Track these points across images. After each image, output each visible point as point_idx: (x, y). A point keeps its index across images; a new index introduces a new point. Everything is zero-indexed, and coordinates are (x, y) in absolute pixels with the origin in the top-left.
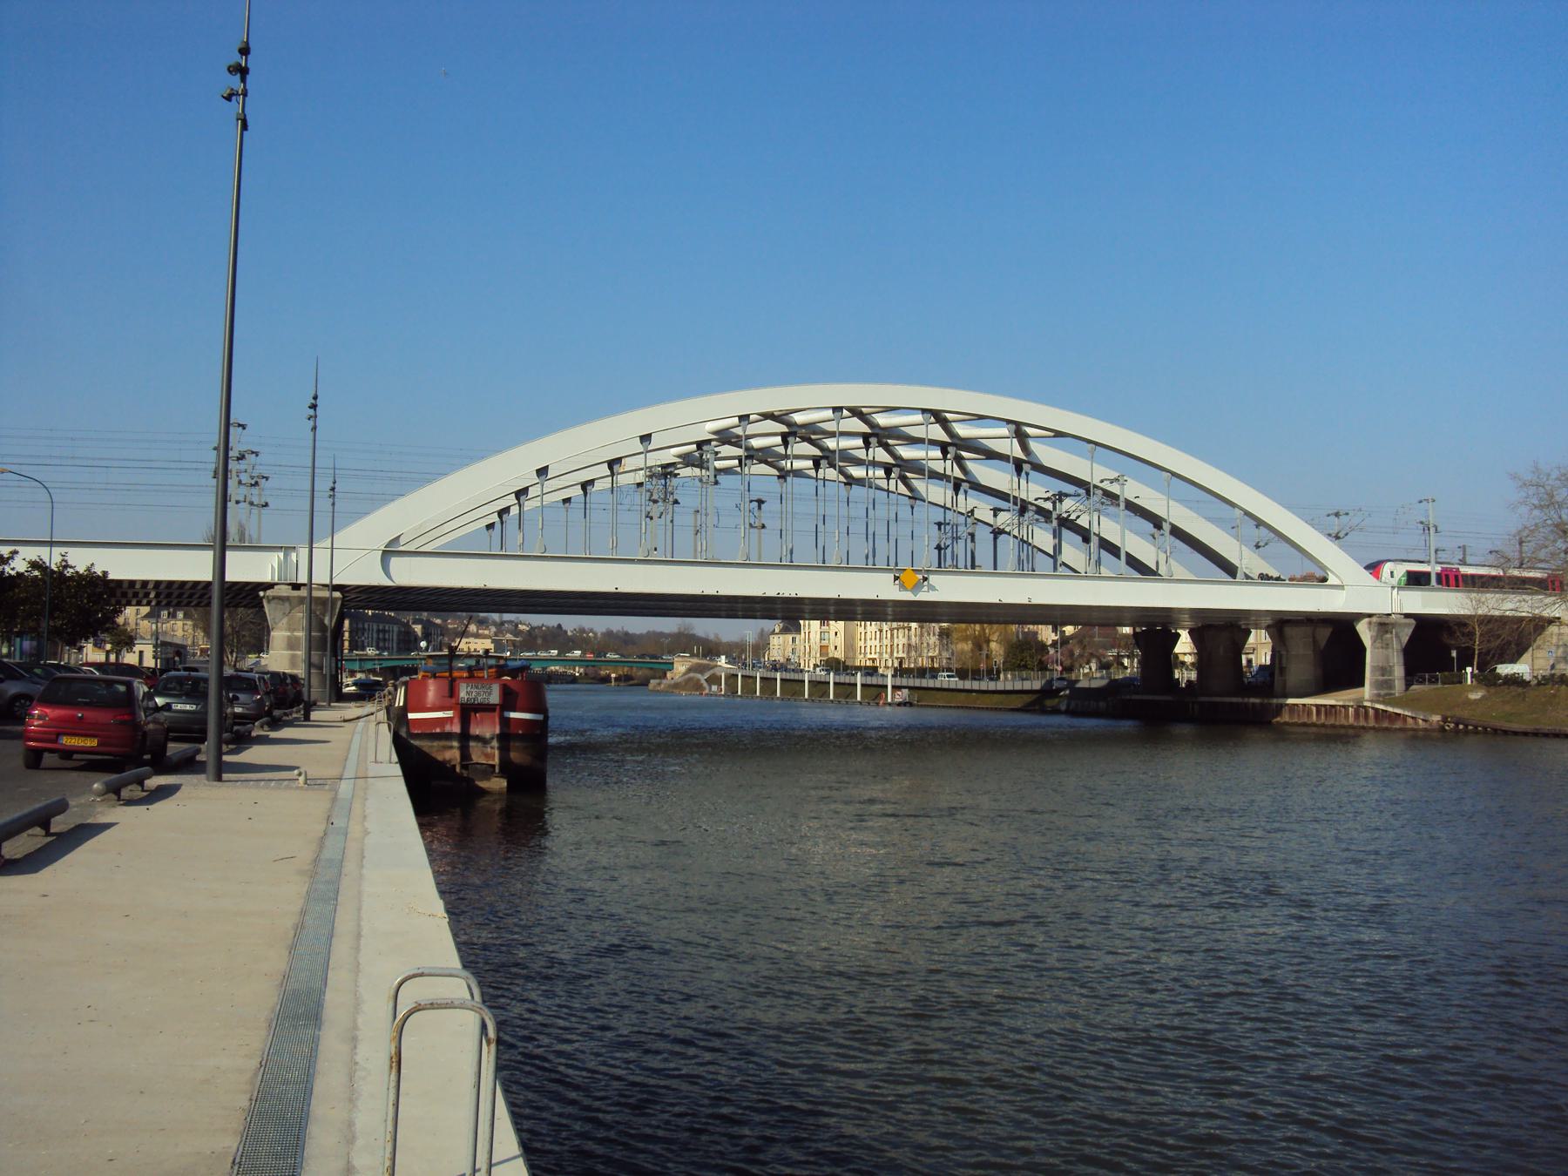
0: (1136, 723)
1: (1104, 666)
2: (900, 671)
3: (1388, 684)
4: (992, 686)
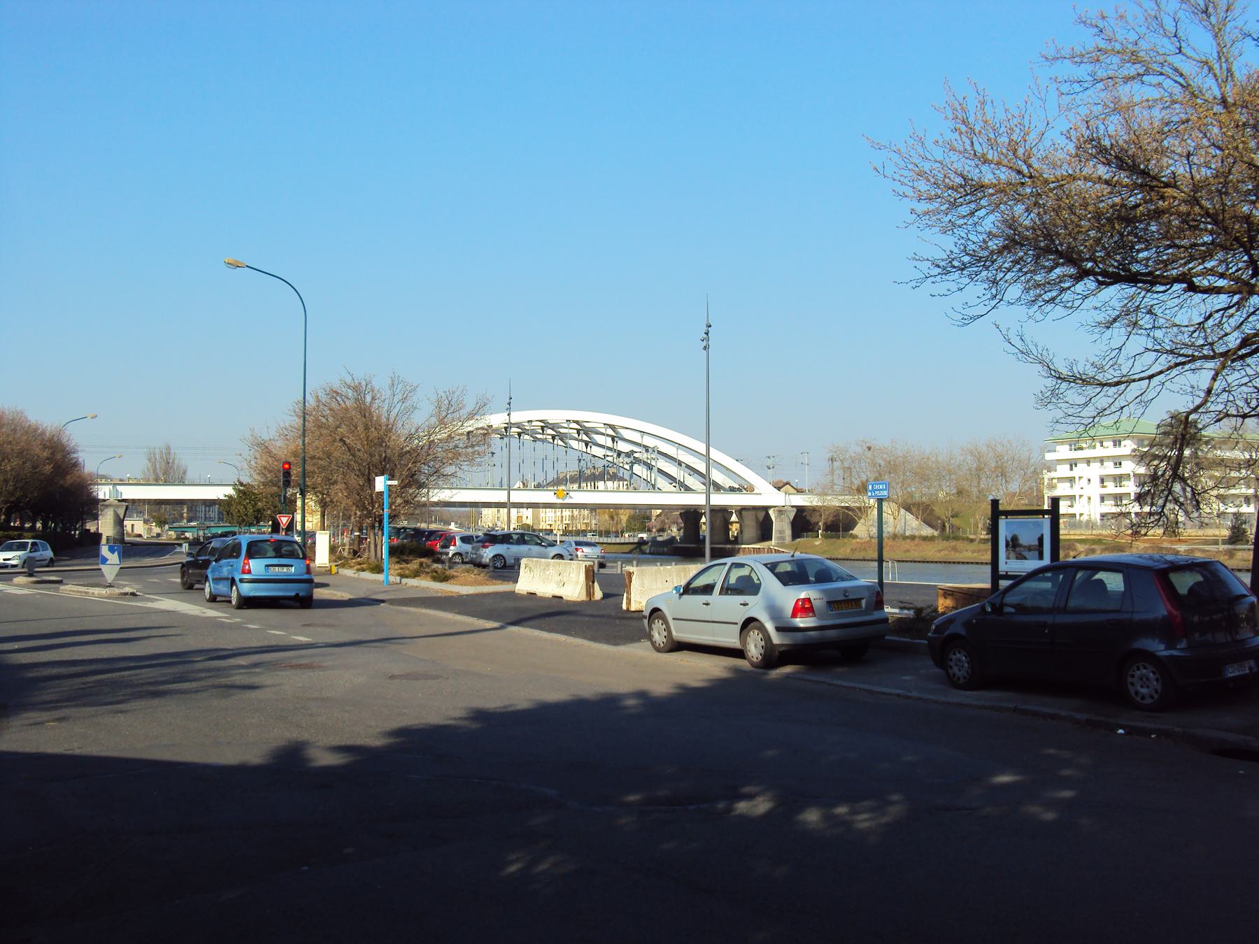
0: (1122, 589)
1: (276, 528)
2: (566, 533)
3: (783, 538)
4: (618, 540)
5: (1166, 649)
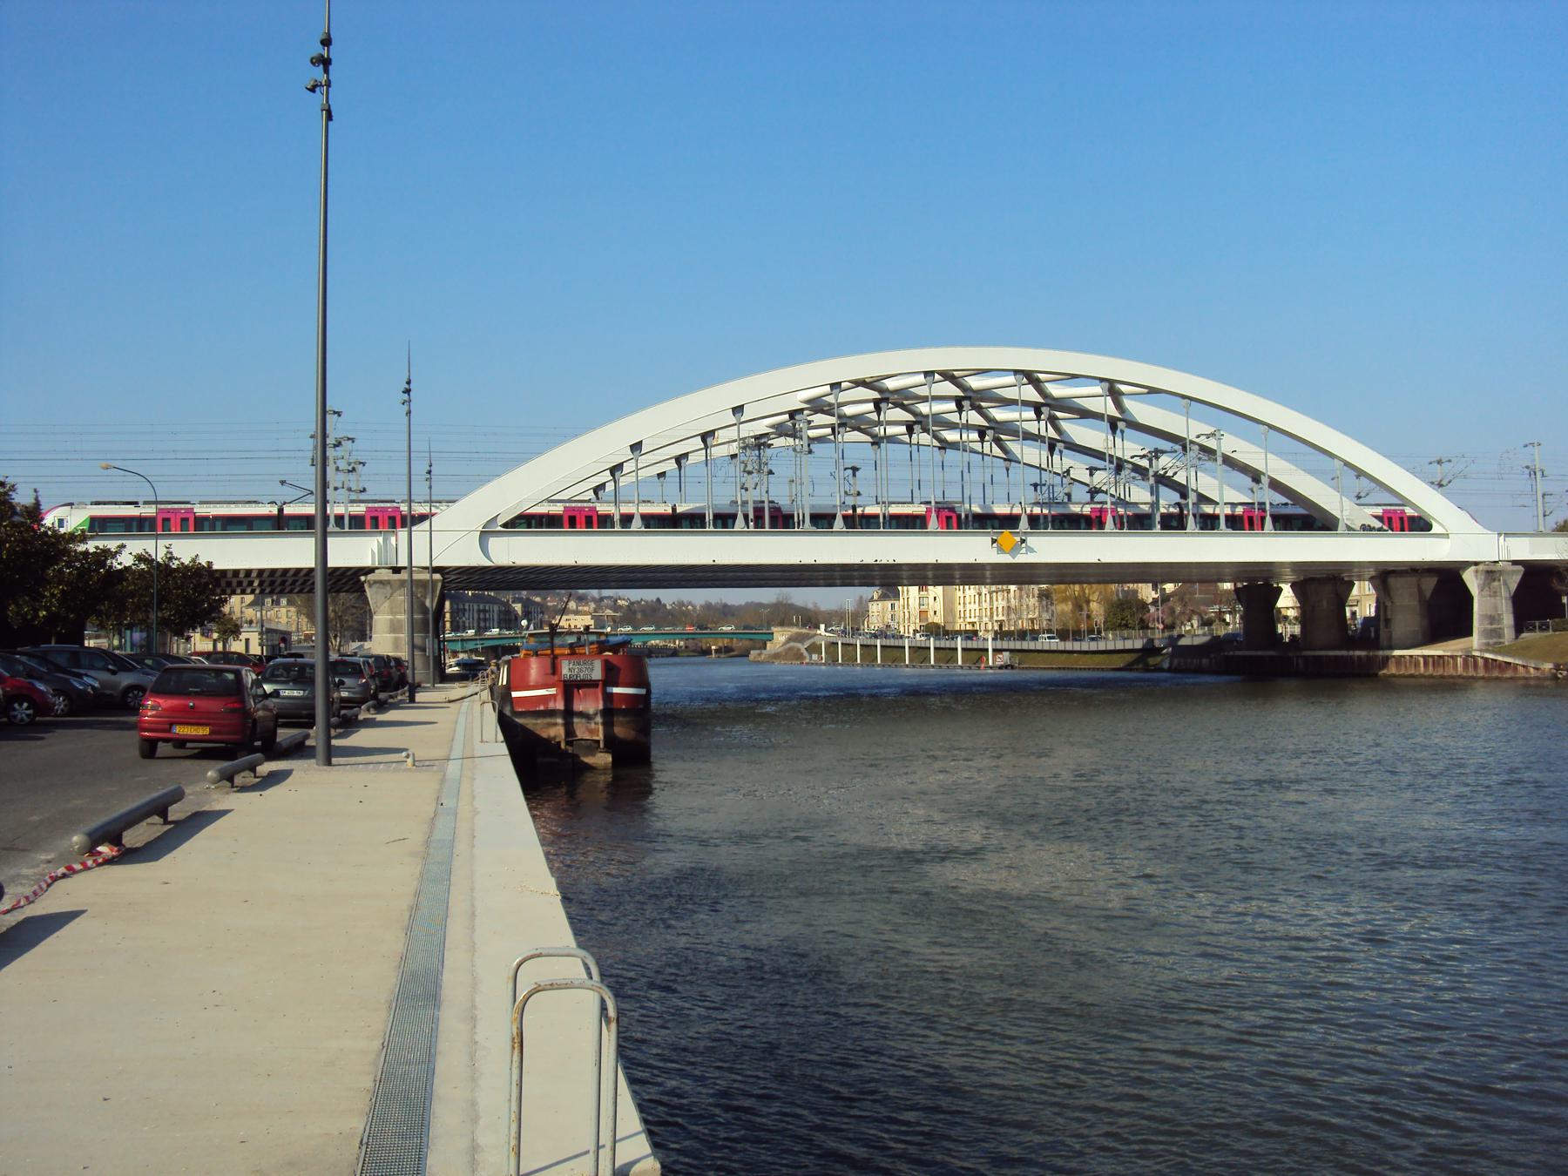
2: (1001, 634)
3: (1497, 633)
4: (1093, 646)
5: (106, 553)
